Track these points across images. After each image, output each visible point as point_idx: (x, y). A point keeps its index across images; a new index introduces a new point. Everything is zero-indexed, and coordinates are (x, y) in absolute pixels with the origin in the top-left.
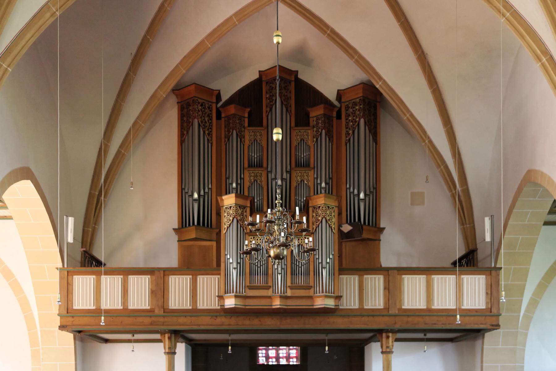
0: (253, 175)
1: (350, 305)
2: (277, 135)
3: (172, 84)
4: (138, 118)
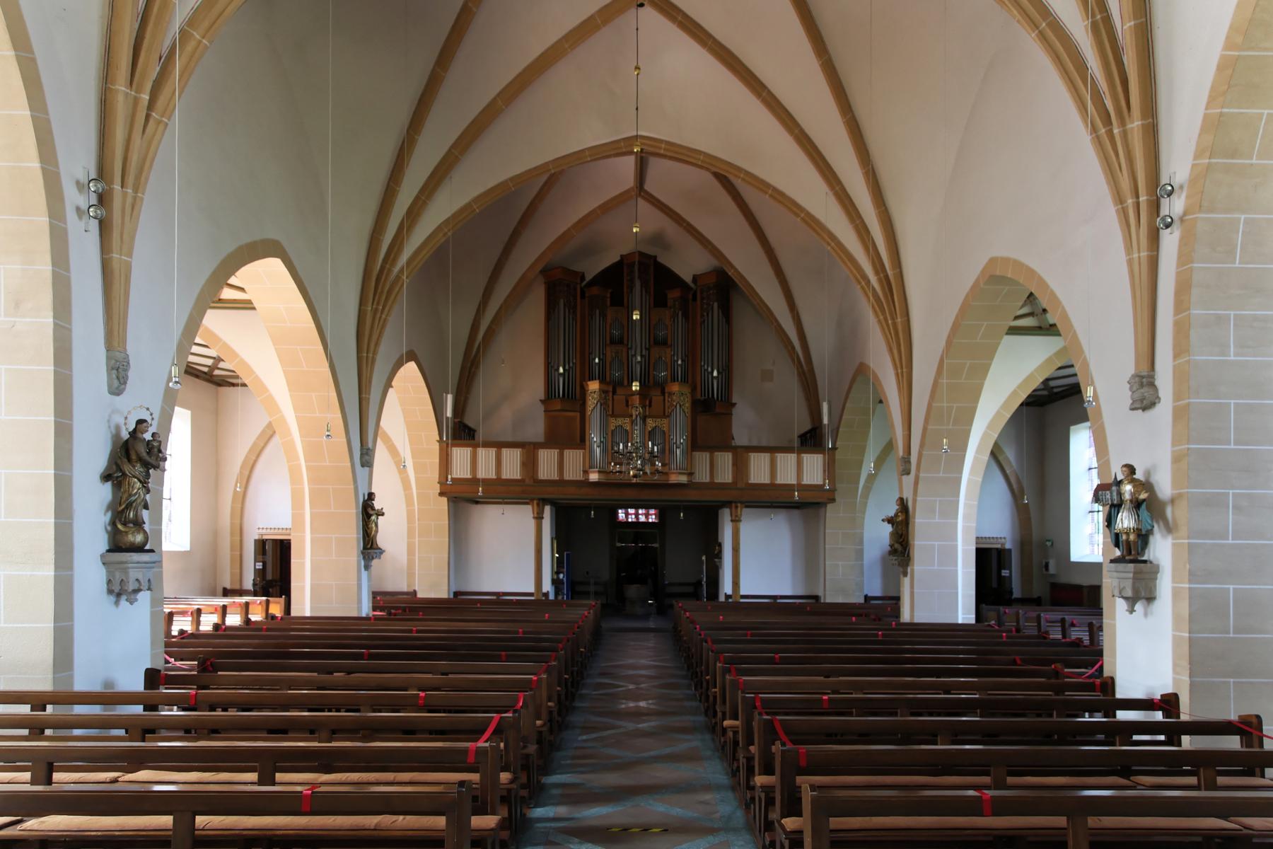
2: (636, 317)
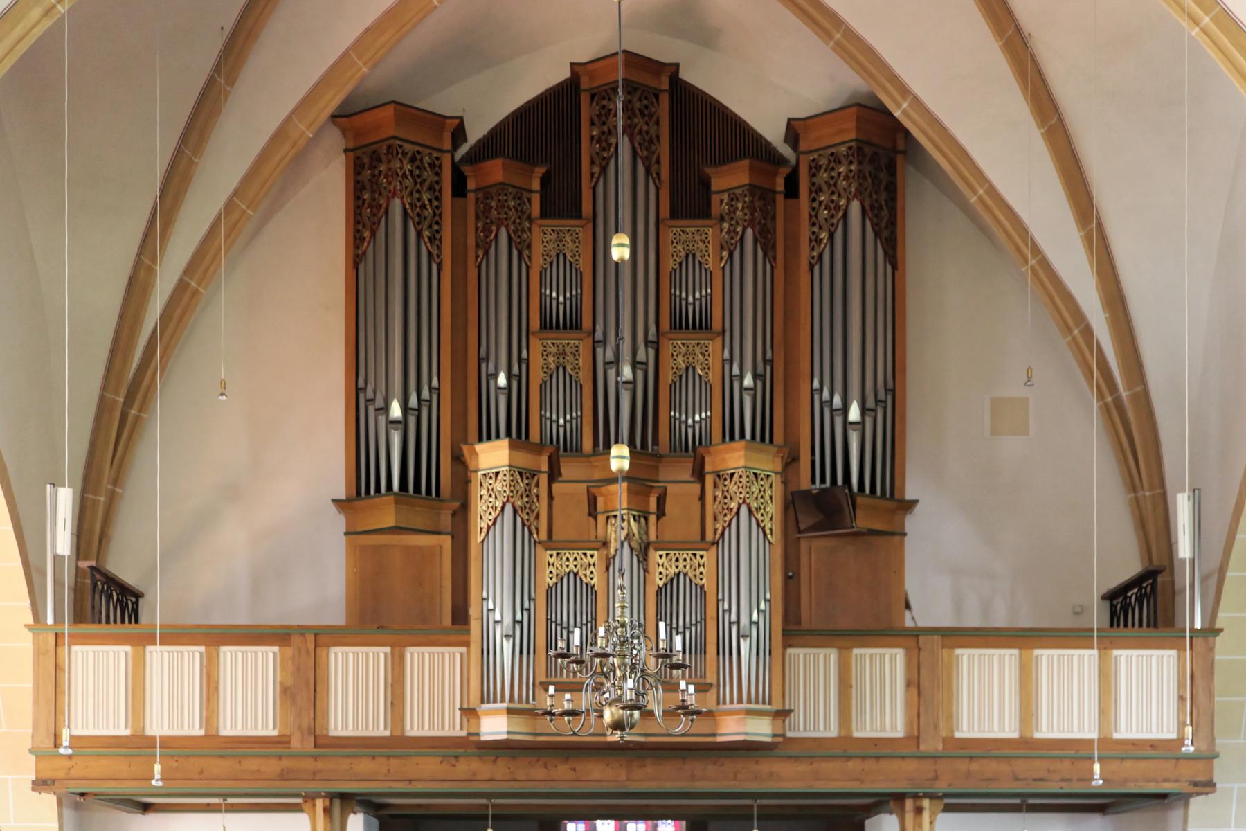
0: (554, 350)
1: (816, 728)
2: (620, 250)
3: (332, 101)
4: (236, 193)
